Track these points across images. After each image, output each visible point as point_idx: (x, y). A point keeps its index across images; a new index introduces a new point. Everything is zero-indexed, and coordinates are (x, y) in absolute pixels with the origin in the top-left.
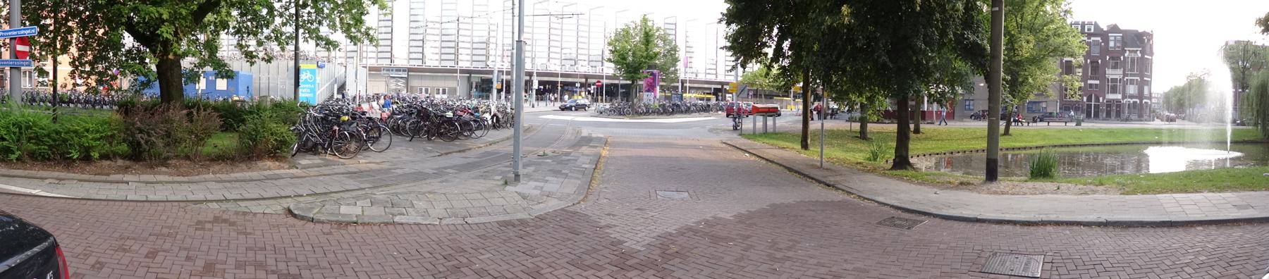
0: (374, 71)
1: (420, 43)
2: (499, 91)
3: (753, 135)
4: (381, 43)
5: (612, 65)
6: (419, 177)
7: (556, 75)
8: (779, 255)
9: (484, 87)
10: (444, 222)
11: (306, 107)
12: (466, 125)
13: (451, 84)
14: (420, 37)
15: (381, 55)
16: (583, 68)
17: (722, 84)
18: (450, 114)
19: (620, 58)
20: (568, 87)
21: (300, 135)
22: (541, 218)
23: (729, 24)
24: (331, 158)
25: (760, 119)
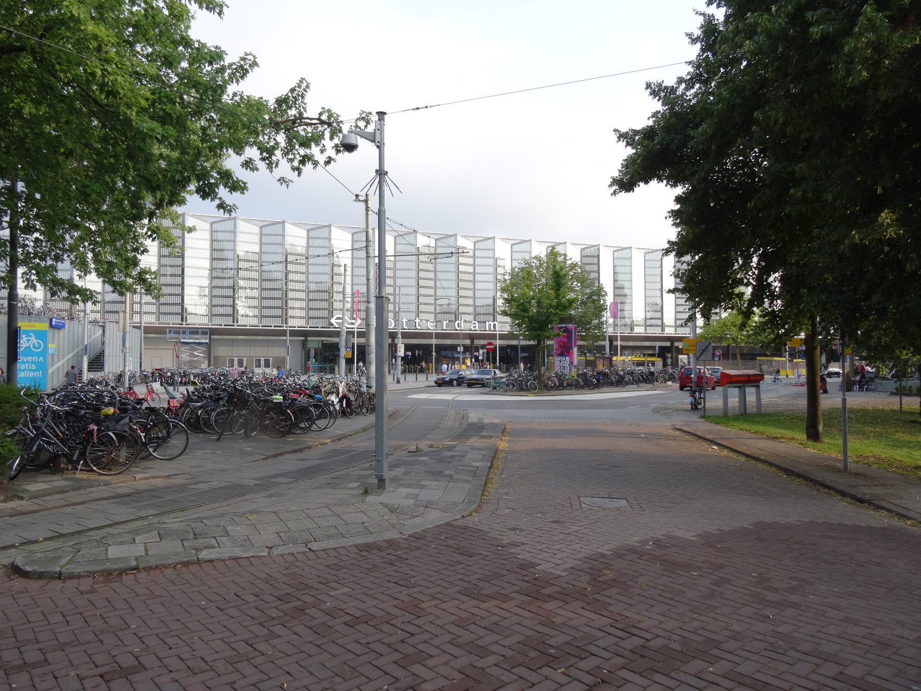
0: (153, 334)
1: (229, 292)
2: (349, 361)
3: (725, 417)
4: (165, 290)
5: (508, 319)
6: (236, 491)
7: (428, 336)
8: (772, 597)
9: (327, 355)
10: (275, 552)
11: (34, 394)
12: (303, 413)
13: (277, 352)
14: (229, 283)
15: (164, 309)
16: (467, 325)
17: (672, 339)
18: (278, 398)
19: (518, 308)
20: (447, 353)
21: (26, 443)
22: (416, 537)
23: (680, 254)
24: (85, 476)
25: (734, 392)
